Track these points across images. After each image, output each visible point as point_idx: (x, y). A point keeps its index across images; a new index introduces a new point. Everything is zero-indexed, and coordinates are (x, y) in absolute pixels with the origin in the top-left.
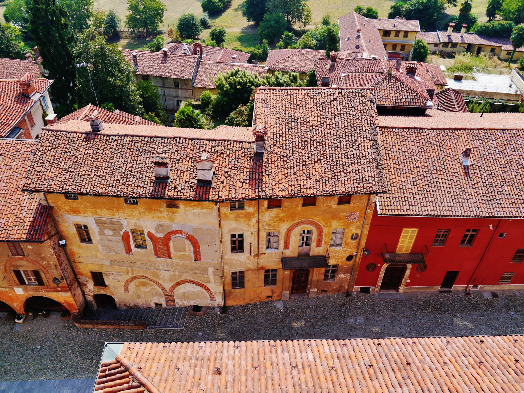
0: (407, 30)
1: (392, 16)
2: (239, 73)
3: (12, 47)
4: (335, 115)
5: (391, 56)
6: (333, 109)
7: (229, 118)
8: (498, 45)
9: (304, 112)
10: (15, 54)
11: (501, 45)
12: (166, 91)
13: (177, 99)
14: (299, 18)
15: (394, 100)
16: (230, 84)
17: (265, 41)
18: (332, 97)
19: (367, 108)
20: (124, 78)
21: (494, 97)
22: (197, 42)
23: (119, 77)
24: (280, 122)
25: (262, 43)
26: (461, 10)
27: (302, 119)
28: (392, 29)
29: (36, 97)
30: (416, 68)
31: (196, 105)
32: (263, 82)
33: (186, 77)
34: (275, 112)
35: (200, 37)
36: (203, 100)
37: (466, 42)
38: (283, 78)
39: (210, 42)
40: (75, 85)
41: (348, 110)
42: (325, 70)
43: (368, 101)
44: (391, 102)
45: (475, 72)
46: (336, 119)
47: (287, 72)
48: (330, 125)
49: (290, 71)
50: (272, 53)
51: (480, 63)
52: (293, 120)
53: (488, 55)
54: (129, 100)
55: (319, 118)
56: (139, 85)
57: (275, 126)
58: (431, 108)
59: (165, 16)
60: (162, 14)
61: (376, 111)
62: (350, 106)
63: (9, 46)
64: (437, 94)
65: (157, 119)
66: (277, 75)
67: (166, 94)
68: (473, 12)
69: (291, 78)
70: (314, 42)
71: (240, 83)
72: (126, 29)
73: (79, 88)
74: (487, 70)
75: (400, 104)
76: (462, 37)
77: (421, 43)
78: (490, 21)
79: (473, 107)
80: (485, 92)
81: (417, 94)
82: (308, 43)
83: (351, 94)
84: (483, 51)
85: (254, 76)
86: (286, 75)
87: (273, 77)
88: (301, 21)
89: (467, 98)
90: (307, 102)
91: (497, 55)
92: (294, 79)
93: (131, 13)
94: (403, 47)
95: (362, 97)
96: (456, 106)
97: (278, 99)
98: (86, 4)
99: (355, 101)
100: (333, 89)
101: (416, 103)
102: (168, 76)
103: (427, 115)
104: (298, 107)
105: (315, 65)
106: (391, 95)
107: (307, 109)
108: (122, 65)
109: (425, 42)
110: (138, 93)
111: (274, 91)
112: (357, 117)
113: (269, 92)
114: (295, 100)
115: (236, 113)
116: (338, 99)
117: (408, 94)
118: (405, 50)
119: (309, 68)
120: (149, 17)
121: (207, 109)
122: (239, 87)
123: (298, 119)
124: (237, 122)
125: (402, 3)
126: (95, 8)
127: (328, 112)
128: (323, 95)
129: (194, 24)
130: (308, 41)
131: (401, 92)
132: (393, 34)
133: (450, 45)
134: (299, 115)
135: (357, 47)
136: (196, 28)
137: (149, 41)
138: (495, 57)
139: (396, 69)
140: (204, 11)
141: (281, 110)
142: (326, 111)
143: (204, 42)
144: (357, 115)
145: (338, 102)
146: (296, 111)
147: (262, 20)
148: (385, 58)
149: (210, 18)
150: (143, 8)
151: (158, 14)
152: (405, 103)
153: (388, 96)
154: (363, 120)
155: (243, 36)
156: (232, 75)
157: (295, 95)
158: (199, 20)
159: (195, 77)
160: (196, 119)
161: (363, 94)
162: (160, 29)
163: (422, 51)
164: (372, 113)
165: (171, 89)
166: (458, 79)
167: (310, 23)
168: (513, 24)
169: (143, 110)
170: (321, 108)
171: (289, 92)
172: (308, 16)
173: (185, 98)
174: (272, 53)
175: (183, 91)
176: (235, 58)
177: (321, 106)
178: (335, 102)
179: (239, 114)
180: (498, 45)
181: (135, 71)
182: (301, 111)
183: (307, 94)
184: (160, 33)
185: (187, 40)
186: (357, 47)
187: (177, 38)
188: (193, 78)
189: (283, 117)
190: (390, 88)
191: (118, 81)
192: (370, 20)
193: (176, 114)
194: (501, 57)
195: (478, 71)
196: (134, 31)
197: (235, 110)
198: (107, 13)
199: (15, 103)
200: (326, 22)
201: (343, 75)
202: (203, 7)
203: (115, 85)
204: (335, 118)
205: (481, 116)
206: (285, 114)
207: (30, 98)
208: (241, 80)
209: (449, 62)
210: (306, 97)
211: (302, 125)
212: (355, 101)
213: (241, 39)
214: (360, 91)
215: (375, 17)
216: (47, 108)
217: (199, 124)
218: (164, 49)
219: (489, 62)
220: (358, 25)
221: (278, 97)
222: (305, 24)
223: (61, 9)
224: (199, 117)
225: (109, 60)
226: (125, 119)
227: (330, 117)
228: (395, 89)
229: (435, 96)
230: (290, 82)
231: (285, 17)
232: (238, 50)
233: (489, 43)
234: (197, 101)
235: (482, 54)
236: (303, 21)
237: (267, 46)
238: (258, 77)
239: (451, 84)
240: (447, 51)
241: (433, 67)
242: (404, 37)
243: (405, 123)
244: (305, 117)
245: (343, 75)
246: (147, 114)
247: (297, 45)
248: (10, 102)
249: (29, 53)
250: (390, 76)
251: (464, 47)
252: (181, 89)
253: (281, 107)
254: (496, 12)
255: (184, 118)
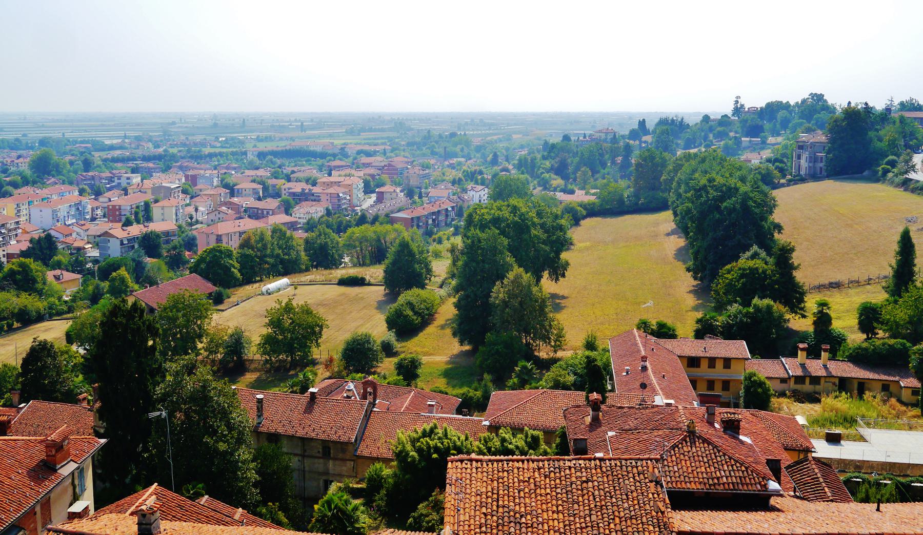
0: (728, 355)
1: (699, 335)
2: (436, 431)
3: (61, 383)
4: (590, 510)
5: (703, 400)
6: (586, 497)
7: (415, 514)
8: (892, 378)
9: (533, 504)
10: (62, 394)
11: (897, 378)
12: (307, 462)
13: (325, 478)
14: (546, 338)
15: (706, 480)
16: (419, 451)
17: (487, 377)
18: (584, 474)
19: (651, 496)
20: (232, 438)
21: (909, 472)
22: (370, 378)
23: (225, 436)
24: (489, 522)
25: (482, 380)
26: (815, 323)
27: (529, 517)
28: (702, 355)
29: (67, 469)
30: (739, 421)
31: (358, 488)
32: (478, 447)
33: (344, 439)
34: (478, 503)
35: (378, 370)
36: (371, 480)
37: (834, 374)
38: (514, 441)
39: (394, 377)
40: (145, 450)
41: (614, 500)
42: (583, 426)
43: (651, 481)
44: (700, 483)
45: (860, 426)
46: (594, 518)
47: (521, 430)
48: (581, 528)
49: (526, 428)
50: (495, 395)
51: (868, 410)
52: (512, 519)
53: (879, 397)
54: (237, 479)
55: (561, 516)
56: (258, 450)
57: (478, 530)
58: (778, 494)
59: (324, 337)
60: (320, 333)
61: (668, 501)
62: (618, 492)
63: (56, 381)
64: (787, 468)
65: (281, 516)
66: (504, 435)
67: (307, 469)
68: (837, 325)
69: (529, 440)
70: (571, 378)
71: (437, 449)
72: (258, 357)
73: (151, 455)
74: (883, 423)
75: (717, 487)
76: (825, 366)
77: (755, 378)
78: (868, 338)
79: (867, 491)
80: (890, 463)
81: (747, 468)
82: (562, 380)
83: (618, 468)
84: (870, 390)
85: (463, 438)
86: (519, 436)
87: (496, 439)
88: (549, 343)
89: (856, 474)
90: (538, 484)
91: (895, 396)
92: (534, 444)
93: (270, 330)
94: (726, 385)
95: (639, 474)
96: (827, 490)
97: (485, 479)
98: (200, 318)
99: (627, 482)
100: (595, 459)
101: (747, 485)
102: (313, 435)
103: (774, 509)
104: (522, 494)
105: (565, 416)
106: (699, 470)
107: (539, 498)
108: (234, 415)
109: (762, 376)
110: (252, 465)
111: (479, 464)
112: (633, 513)
113: (469, 466)
114: (516, 480)
115: (428, 506)
116: (595, 478)
117: (730, 468)
118: (731, 389)
119: (556, 421)
120: (297, 338)
121: (377, 498)
122: (435, 456)
123: (522, 516)
124: (428, 522)
125: (714, 314)
126: (213, 324)
127: (578, 503)
128: (568, 472)
129: (370, 350)
130: (560, 376)
131: (716, 465)
132: (704, 364)
133: (808, 380)
134: (523, 509)
135: (643, 386)
136: (373, 355)
137: (292, 377)
138: (893, 400)
139: (708, 422)
140: (390, 328)
141: (490, 500)
142: (574, 502)
143: (385, 378)
144: (632, 509)
145: (596, 483)
146: (517, 501)
147: (483, 343)
148: (695, 403)
149: (397, 340)
150: (291, 324)
151: (314, 333)
152: (726, 486)
153: (693, 473)
154: (644, 520)
155: (451, 369)
156: (425, 434)
157: (516, 471)
158: (379, 342)
159: (360, 438)
160: (352, 517)
161: (640, 468)
162: (314, 357)
163: (760, 390)
164: (661, 505)
165: (316, 460)
166: (834, 439)
167: (564, 347)
168: (908, 344)
169: (259, 498)
170: (564, 495)
171: (505, 465)
172: (559, 336)
173: (339, 477)
174: (495, 395)
175: (337, 462)
176: (433, 406)
177: (564, 491)
178: (590, 484)
179: (433, 507)
180: (892, 378)
181: (257, 427)
182: (527, 500)
183: (539, 469)
184: (314, 363)
185: (354, 375)
186: (643, 386)
187: (339, 372)
188: (356, 440)
189: (494, 513)
190: (696, 458)
191: (221, 444)
192: (662, 341)
193: (316, 507)
194: (904, 399)
195: (868, 425)
196: (271, 359)
197: (427, 500)
198: (230, 331)
199: (27, 480)
200: (590, 346)
201: (610, 434)
202: (387, 322)
203: (216, 450)
204: (590, 515)
205: (878, 510)
206: (498, 506)
207: (56, 471)
208: (439, 445)
209: (812, 409)
210: (537, 474)
211: (530, 529)
212: (627, 482)
213: (447, 374)
214: (634, 463)
215: (673, 336)
216: (83, 490)
217: (357, 526)
218: (312, 390)
219: (885, 409)
220: (642, 349)
221: (485, 474)
222: (556, 348)
223: (150, 324)
224: (358, 513)
225: (213, 406)
226: (212, 514)
227: (582, 514)
228: (705, 460)
229: (784, 472)
230: (526, 448)
231: (521, 338)
232: (441, 392)
233: (876, 376)
234: (358, 483)
235: (867, 395)
236: (553, 344)
237: (490, 385)
238: (471, 439)
239: (822, 449)
240: (806, 390)
241: (782, 418)
242: (724, 368)
243: (729, 524)
244: (534, 513)
245: (610, 434)
246: (265, 505)
247: (543, 383)
248: (19, 477)
249: (86, 393)
250: (692, 435)
251: (834, 384)
252: (335, 459)
253: (490, 494)
254: (875, 325)
255: (329, 514)
